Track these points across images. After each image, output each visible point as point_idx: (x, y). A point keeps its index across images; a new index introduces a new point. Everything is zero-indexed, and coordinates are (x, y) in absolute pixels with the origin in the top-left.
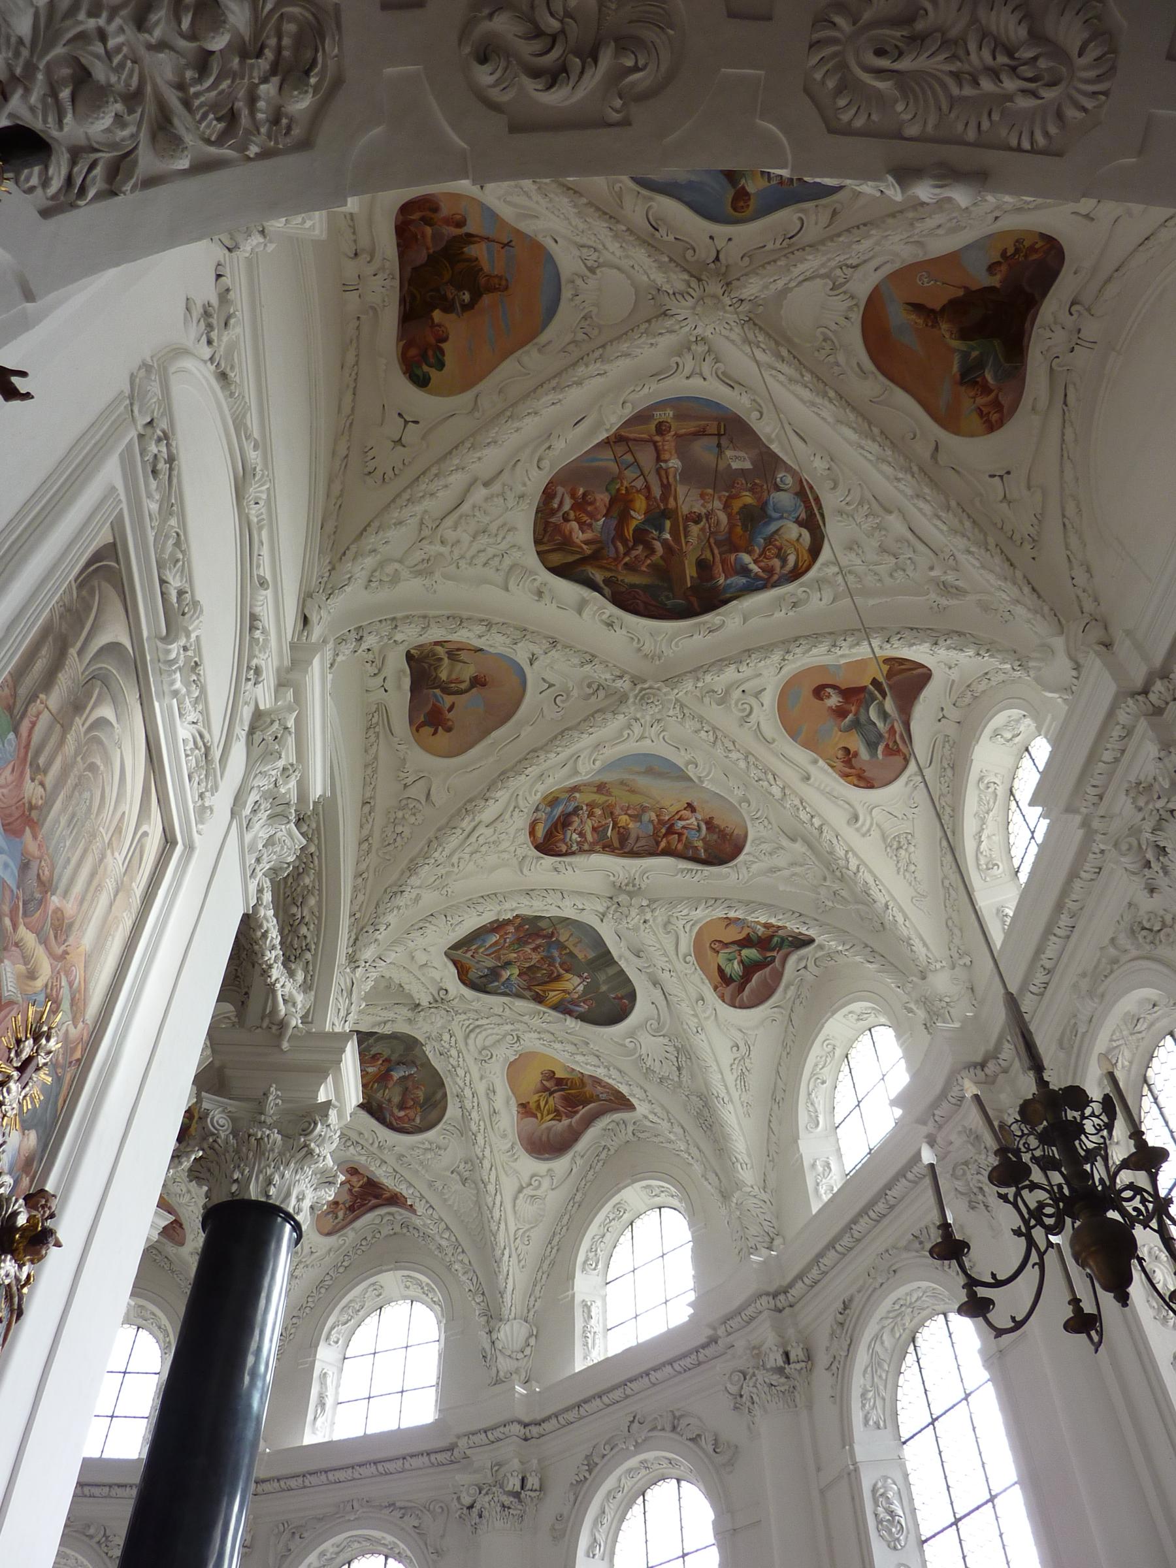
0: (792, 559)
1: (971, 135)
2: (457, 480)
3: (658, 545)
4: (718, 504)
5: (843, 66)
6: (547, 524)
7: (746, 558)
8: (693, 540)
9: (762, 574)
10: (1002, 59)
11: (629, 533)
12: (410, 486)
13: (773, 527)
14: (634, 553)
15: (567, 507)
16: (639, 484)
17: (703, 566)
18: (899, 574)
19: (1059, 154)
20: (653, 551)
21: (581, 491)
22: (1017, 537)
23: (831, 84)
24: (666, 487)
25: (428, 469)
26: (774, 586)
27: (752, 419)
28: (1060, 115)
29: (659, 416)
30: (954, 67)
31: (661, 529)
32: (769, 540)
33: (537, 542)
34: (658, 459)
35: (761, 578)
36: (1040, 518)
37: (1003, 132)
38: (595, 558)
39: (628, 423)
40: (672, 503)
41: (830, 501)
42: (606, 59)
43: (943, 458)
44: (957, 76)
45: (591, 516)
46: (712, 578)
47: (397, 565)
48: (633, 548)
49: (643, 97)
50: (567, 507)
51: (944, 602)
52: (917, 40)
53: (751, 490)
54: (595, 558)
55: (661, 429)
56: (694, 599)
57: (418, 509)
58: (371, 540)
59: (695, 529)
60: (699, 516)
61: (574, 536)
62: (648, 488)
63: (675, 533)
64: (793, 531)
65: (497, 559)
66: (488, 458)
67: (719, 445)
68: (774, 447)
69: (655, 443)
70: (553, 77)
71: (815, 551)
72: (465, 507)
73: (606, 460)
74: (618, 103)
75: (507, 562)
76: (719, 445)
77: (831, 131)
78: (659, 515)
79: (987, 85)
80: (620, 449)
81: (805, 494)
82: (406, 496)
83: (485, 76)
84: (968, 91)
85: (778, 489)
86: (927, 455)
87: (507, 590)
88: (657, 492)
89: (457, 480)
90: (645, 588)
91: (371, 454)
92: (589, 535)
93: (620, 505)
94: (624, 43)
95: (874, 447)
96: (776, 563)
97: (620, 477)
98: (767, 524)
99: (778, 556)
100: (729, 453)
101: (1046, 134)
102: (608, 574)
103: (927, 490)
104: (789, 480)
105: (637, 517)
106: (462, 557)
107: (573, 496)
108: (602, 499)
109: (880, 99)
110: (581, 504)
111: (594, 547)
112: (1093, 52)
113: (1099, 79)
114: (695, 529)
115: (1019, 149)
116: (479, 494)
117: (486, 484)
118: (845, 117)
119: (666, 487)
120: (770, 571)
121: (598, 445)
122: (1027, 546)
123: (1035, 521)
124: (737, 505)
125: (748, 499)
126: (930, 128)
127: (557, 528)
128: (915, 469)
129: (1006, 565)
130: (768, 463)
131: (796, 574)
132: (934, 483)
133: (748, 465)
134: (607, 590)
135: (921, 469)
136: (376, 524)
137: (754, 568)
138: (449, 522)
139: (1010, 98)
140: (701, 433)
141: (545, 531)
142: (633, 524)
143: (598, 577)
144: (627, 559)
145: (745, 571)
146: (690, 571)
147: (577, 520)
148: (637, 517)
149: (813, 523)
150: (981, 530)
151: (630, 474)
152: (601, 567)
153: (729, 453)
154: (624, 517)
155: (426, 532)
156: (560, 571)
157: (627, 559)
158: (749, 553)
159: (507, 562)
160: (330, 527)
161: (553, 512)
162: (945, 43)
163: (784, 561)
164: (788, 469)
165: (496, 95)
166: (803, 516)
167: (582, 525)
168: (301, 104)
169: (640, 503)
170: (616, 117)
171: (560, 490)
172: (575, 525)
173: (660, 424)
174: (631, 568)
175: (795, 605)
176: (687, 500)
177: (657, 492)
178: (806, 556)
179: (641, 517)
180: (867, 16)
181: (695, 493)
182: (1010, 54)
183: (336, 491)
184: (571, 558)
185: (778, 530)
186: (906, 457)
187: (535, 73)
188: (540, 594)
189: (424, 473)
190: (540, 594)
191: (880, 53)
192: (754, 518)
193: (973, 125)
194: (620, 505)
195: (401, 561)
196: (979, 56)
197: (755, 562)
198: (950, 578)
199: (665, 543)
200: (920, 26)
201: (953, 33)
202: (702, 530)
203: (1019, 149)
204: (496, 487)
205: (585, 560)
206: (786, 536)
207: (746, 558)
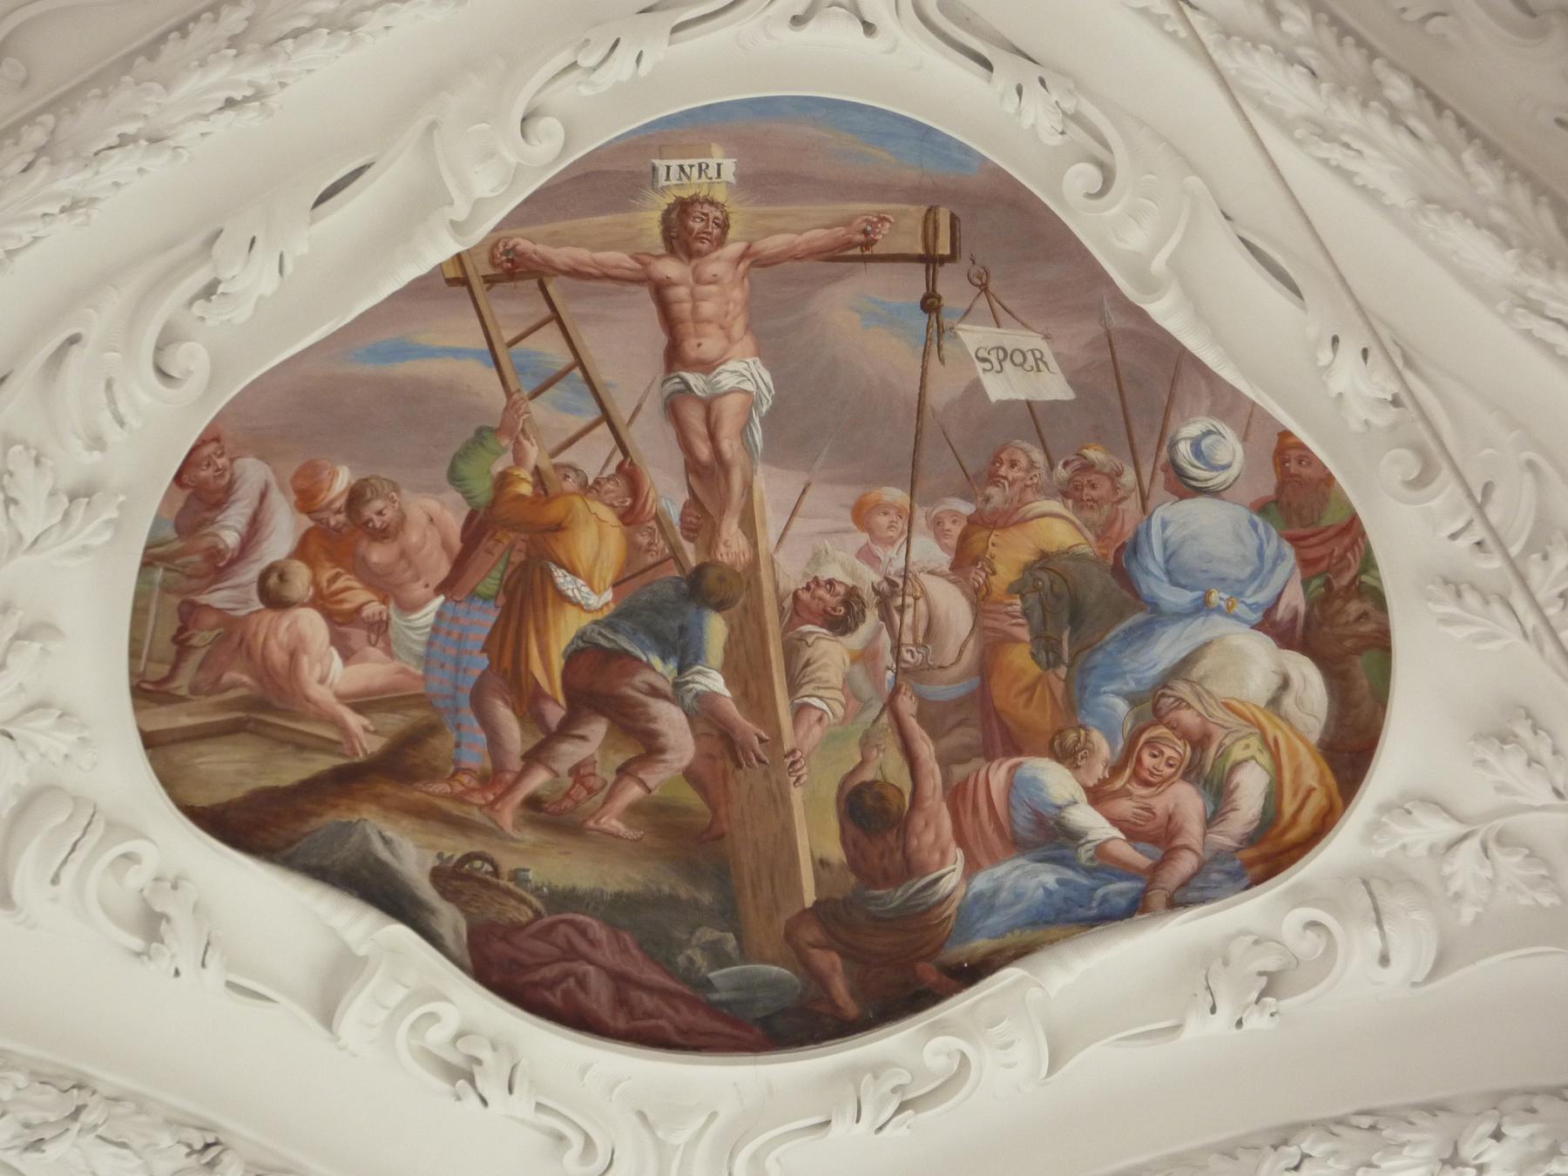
0: (1251, 787)
3: (671, 720)
4: (929, 552)
6: (190, 614)
7: (1057, 782)
8: (827, 700)
11: (547, 665)
13: (1165, 649)
14: (570, 753)
15: (280, 542)
16: (595, 456)
17: (869, 814)
20: (651, 747)
21: (343, 479)
24: (708, 475)
26: (1176, 903)
27: (1069, 196)
29: (677, 176)
31: (685, 652)
33: (145, 692)
34: (674, 357)
35: (1123, 871)
38: (396, 769)
39: (545, 203)
40: (732, 545)
41: (1407, 535)
45: (385, 586)
46: (910, 868)
48: (565, 730)
53: (1068, 492)
54: (396, 769)
55: (685, 230)
56: (829, 962)
59: (831, 655)
60: (852, 597)
61: (309, 672)
62: (630, 475)
63: (746, 669)
64: (1252, 670)
67: (930, 304)
68: (1166, 311)
69: (660, 291)
71: (1350, 750)
76: (930, 304)
78: (679, 595)
80: (513, 310)
81: (1299, 498)
85: (1183, 486)
88: (668, 493)
92: (373, 671)
93: (511, 544)
96: (1187, 801)
97: (510, 428)
98: (1145, 632)
99: (1192, 772)
100: (974, 336)
102: (456, 846)
104: (1230, 449)
105: (586, 597)
107: (306, 500)
108: (432, 515)
110: (344, 535)
111: (395, 722)
119: (708, 475)
120: (1162, 837)
121: (418, 290)
124: (1010, 555)
125: (1057, 529)
127: (234, 637)
130: (1140, 377)
131: (1272, 851)
133: (1053, 387)
134: (450, 919)
140: (852, 252)
141: (182, 644)
142: (566, 628)
143: (412, 855)
144: (538, 780)
145: (1051, 837)
146: (816, 836)
147: (322, 601)
148: (586, 597)
149: (1342, 628)
151: (555, 416)
152: (425, 814)
153: (974, 336)
154: (527, 595)
156: (243, 825)
157: (538, 780)
158: (1068, 756)
161: (219, 566)
163: (1219, 793)
164: (1226, 402)
166: (1295, 599)
167: (341, 621)
171: (253, 472)
172: (311, 624)
173: (683, 207)
175: (1272, 985)
176: (797, 531)
177: (668, 493)
178: (1313, 772)
179: (601, 600)
181: (829, 504)
184: (292, 771)
185: (1188, 662)
188: (151, 924)
190: (151, 924)
192: (1085, 607)
194: (511, 544)
197: (1097, 796)
199: (703, 713)
202: (866, 657)
205: (350, 780)
207: (1057, 782)
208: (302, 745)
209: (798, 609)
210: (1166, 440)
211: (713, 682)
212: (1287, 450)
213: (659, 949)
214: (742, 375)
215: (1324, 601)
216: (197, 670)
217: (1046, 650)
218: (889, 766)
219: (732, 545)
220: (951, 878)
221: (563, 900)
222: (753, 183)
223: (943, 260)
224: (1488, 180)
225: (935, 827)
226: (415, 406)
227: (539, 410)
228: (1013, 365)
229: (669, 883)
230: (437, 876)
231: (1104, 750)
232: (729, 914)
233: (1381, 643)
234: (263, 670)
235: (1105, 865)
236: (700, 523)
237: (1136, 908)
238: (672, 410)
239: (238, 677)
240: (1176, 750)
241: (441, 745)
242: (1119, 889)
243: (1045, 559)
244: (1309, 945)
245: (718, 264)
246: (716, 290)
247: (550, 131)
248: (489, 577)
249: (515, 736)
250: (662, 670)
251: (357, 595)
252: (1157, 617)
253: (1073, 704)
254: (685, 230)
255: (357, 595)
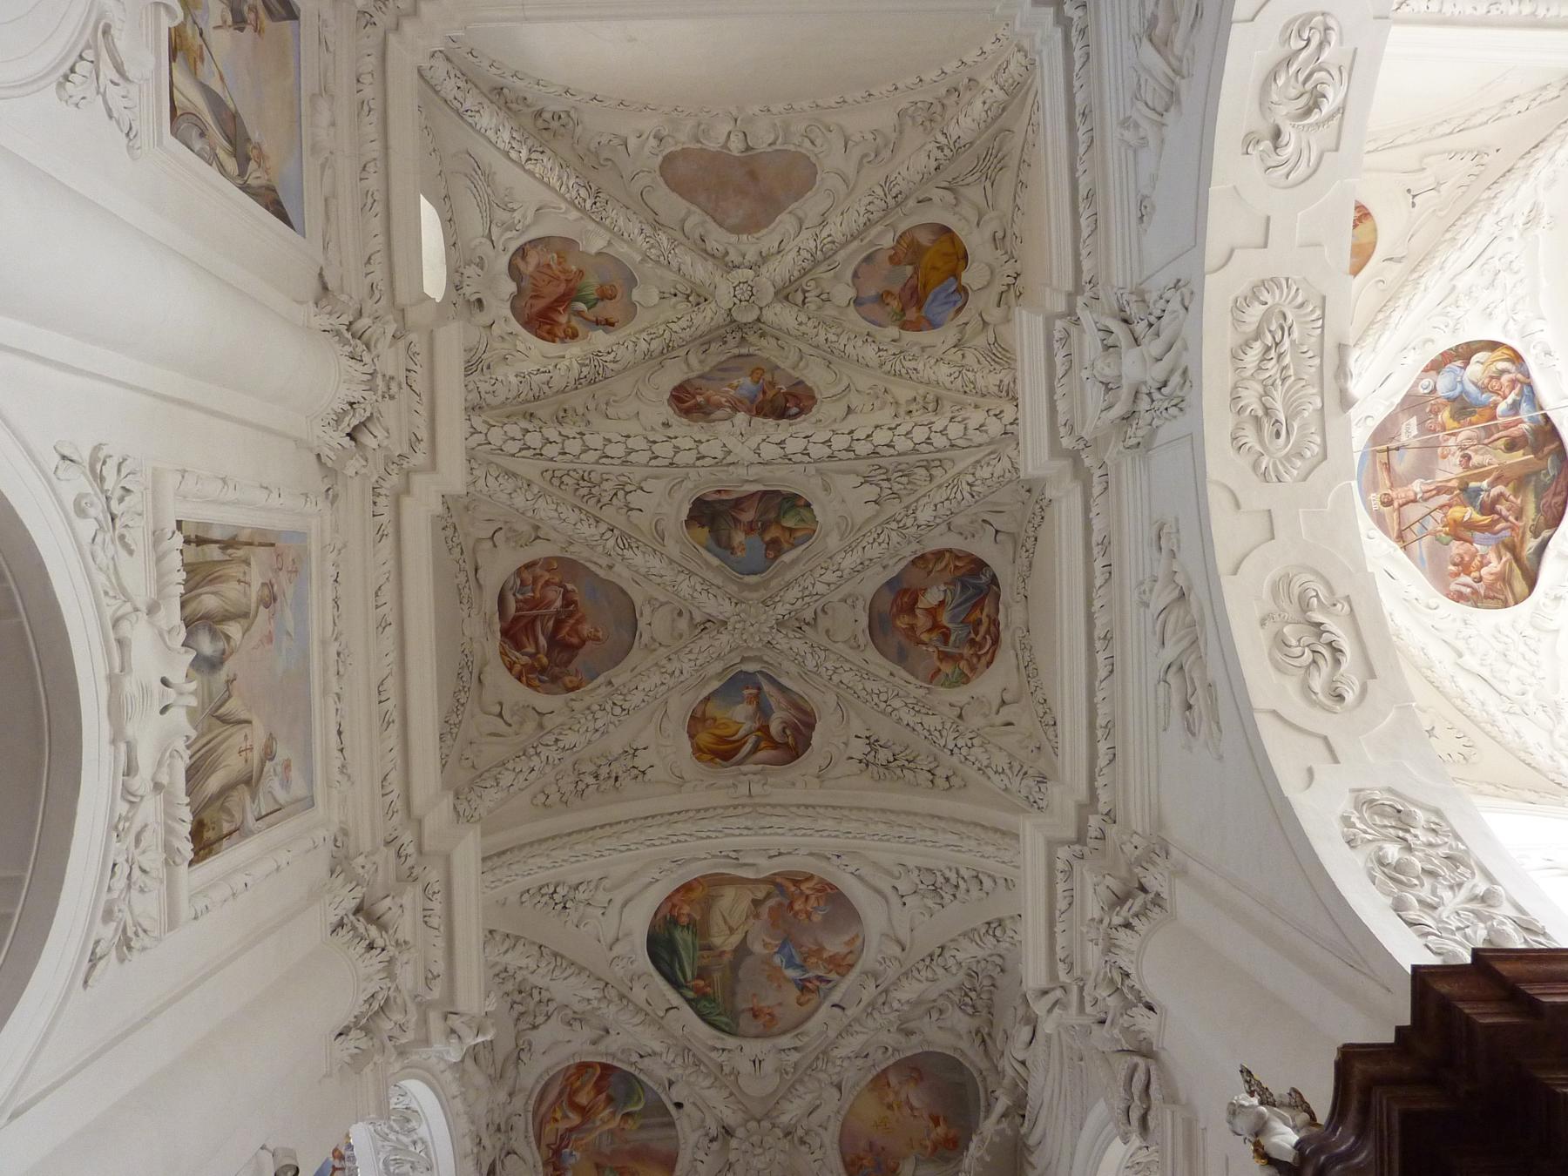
0: (1502, 365)
1: (1317, 361)
2: (1465, 683)
3: (1494, 492)
4: (1452, 441)
5: (1287, 457)
6: (1487, 597)
7: (1502, 407)
8: (1486, 459)
9: (1517, 390)
10: (1273, 354)
11: (1486, 519)
12: (1477, 724)
13: (1471, 389)
14: (1504, 512)
15: (1468, 580)
16: (1438, 515)
17: (1512, 446)
18: (1515, 267)
19: (1324, 298)
20: (1501, 495)
21: (1452, 568)
22: (1476, 170)
23: (1299, 463)
24: (1439, 491)
25: (1456, 708)
26: (1528, 376)
27: (1373, 424)
28: (1302, 305)
29: (1376, 505)
30: (1279, 382)
31: (1478, 491)
32: (1483, 389)
33: (1506, 605)
34: (1415, 501)
35: (1522, 390)
36: (1453, 154)
37: (1313, 340)
38: (1513, 549)
39: (1386, 532)
40: (1454, 483)
41: (1446, 342)
42: (1318, 617)
43: (1398, 254)
44: (1284, 380)
45: (1473, 556)
46: (1524, 435)
47: (1556, 736)
48: (1499, 514)
49: (1331, 591)
50: (1468, 580)
51: (1545, 220)
52: (1267, 410)
53: (1436, 414)
54: (1513, 549)
55: (1388, 503)
56: (1546, 450)
57: (1500, 717)
58: (1541, 759)
59: (1476, 459)
60: (1463, 456)
61: (1495, 570)
62: (1441, 507)
63: (1481, 477)
64: (1476, 369)
65: (1529, 642)
66: (1440, 656)
67: (1397, 449)
68: (1397, 400)
69: (1401, 506)
70: (1336, 651)
71: (1493, 346)
72: (1486, 673)
73: (1422, 547)
74: (1339, 606)
75: (1529, 632)
76: (1397, 449)
77: (1325, 457)
78: (1467, 494)
79: (1287, 360)
80: (1409, 536)
81: (1436, 366)
82: (1488, 727)
83: (1350, 697)
84: (1291, 372)
85: (1434, 390)
86: (1397, 267)
87: (1557, 631)
88: (1444, 499)
89: (1465, 683)
90: (1538, 497)
91: (1446, 758)
92: (1492, 556)
93: (1460, 531)
94: (1305, 607)
95: (1396, 315)
96: (1505, 378)
97: (1434, 533)
98: (1467, 393)
99: (1498, 378)
100: (1404, 439)
101: (1313, 311)
102: (1529, 534)
103: (1436, 262)
104: (1425, 382)
105: (1469, 513)
106: (1533, 674)
107: (1457, 575)
108: (1456, 548)
109: (1302, 427)
110: (1464, 566)
111: (1503, 551)
112: (1265, 296)
113: (1279, 287)
114: (1476, 459)
115: (1322, 327)
116: (1470, 661)
117: (1460, 655)
118: (1316, 449)
119: (1439, 491)
120: (1514, 382)
121: (1409, 556)
122: (1486, 159)
123: (1458, 157)
124: (1451, 423)
125: (1445, 415)
126: (1315, 391)
127: (1490, 587)
128: (1415, 275)
129: (1511, 176)
130: (1412, 403)
131: (1516, 358)
132: (1428, 256)
133: (1414, 421)
134: (1545, 534)
135: (1414, 270)
136: (1523, 755)
137: (1510, 400)
138: (1501, 687)
139: (1293, 343)
140: (1388, 466)
141: (1494, 598)
142: (1477, 517)
143: (1532, 544)
144: (1511, 518)
145: (1515, 407)
146: (1518, 456)
147: (1479, 569)
148: (1469, 513)
149: (1465, 353)
150: (1473, 205)
151: (1431, 525)
152: (1522, 541)
153: (1404, 439)
154: (1471, 526)
155: (1516, 709)
156: (1532, 582)
157: (1511, 518)
158: (1496, 405)
159: (1529, 632)
160: (1533, 797)
161: (1475, 592)
162: (1266, 394)
163: (1503, 372)
164: (1416, 384)
165: (1357, 688)
166: (1459, 363)
167: (1482, 565)
168: (1421, 816)
169: (1458, 512)
170: (1346, 607)
171: (1453, 587)
172: (1484, 571)
173: (1383, 503)
174: (1519, 515)
175: (1548, 353)
176: (1449, 470)
177: (1444, 499)
178: (1498, 353)
179: (1470, 510)
180: (1259, 448)
181: (1442, 464)
182: (1268, 349)
183: (1491, 789)
184: (1517, 572)
185: (1475, 384)
186: (1403, 286)
187: (1337, 662)
188: (1557, 598)
189: (1461, 711)
190: (1557, 598)
191: (1278, 435)
192: (1463, 408)
193: (1311, 362)
194: (1460, 531)
195: (1551, 733)
196: (1272, 368)
197: (1505, 398)
198: (1520, 220)
199: (1492, 485)
200: (1260, 413)
201: (1261, 390)
202: (1476, 452)
203: (1322, 327)
204: (1460, 645)
205: (1517, 559)
206: (1479, 375)
207: (1502, 407)
208: (1511, 570)
209: (1467, 467)
210: (1423, 396)
211: (1485, 484)
212: (1425, 371)
213: (1546, 487)
214: (1417, 486)
215: (1459, 357)
216: (1497, 595)
217: (1472, 413)
218: (1501, 443)
219: (1454, 483)
220: (1525, 426)
221: (1538, 510)
222: (1375, 491)
223: (1061, 316)
224: (1370, 340)
225: (1514, 431)
226: (1433, 554)
227: (1430, 528)
228: (1409, 430)
229: (1531, 487)
230: (1536, 537)
231: (1495, 398)
232: (1537, 473)
233: (1468, 344)
234: (1496, 580)
235: (1521, 393)
236: (1449, 491)
237: (1530, 385)
238: (1426, 500)
239: (1499, 585)
240: (1494, 382)
241: (1507, 540)
242: (1526, 390)
243: (1452, 417)
244: (1539, 347)
245: (1394, 494)
246: (1399, 494)
247: (1371, 533)
248: (1468, 534)
249: (1502, 525)
250: (1483, 495)
251: (1476, 562)
252: (1464, 391)
253: (1484, 406)
254: (1388, 503)
255: (1476, 562)
